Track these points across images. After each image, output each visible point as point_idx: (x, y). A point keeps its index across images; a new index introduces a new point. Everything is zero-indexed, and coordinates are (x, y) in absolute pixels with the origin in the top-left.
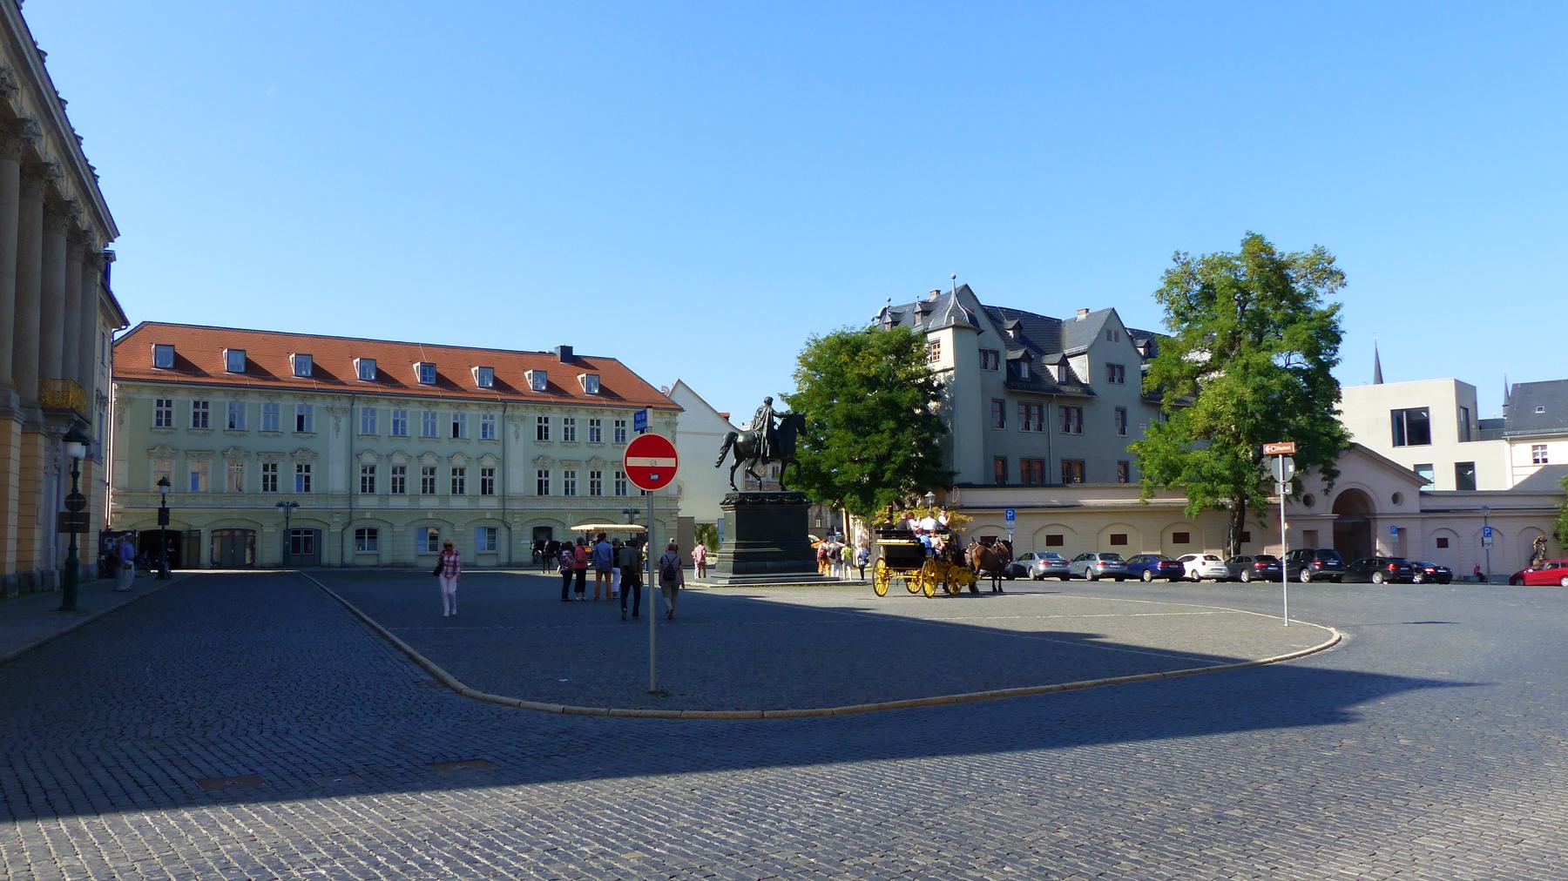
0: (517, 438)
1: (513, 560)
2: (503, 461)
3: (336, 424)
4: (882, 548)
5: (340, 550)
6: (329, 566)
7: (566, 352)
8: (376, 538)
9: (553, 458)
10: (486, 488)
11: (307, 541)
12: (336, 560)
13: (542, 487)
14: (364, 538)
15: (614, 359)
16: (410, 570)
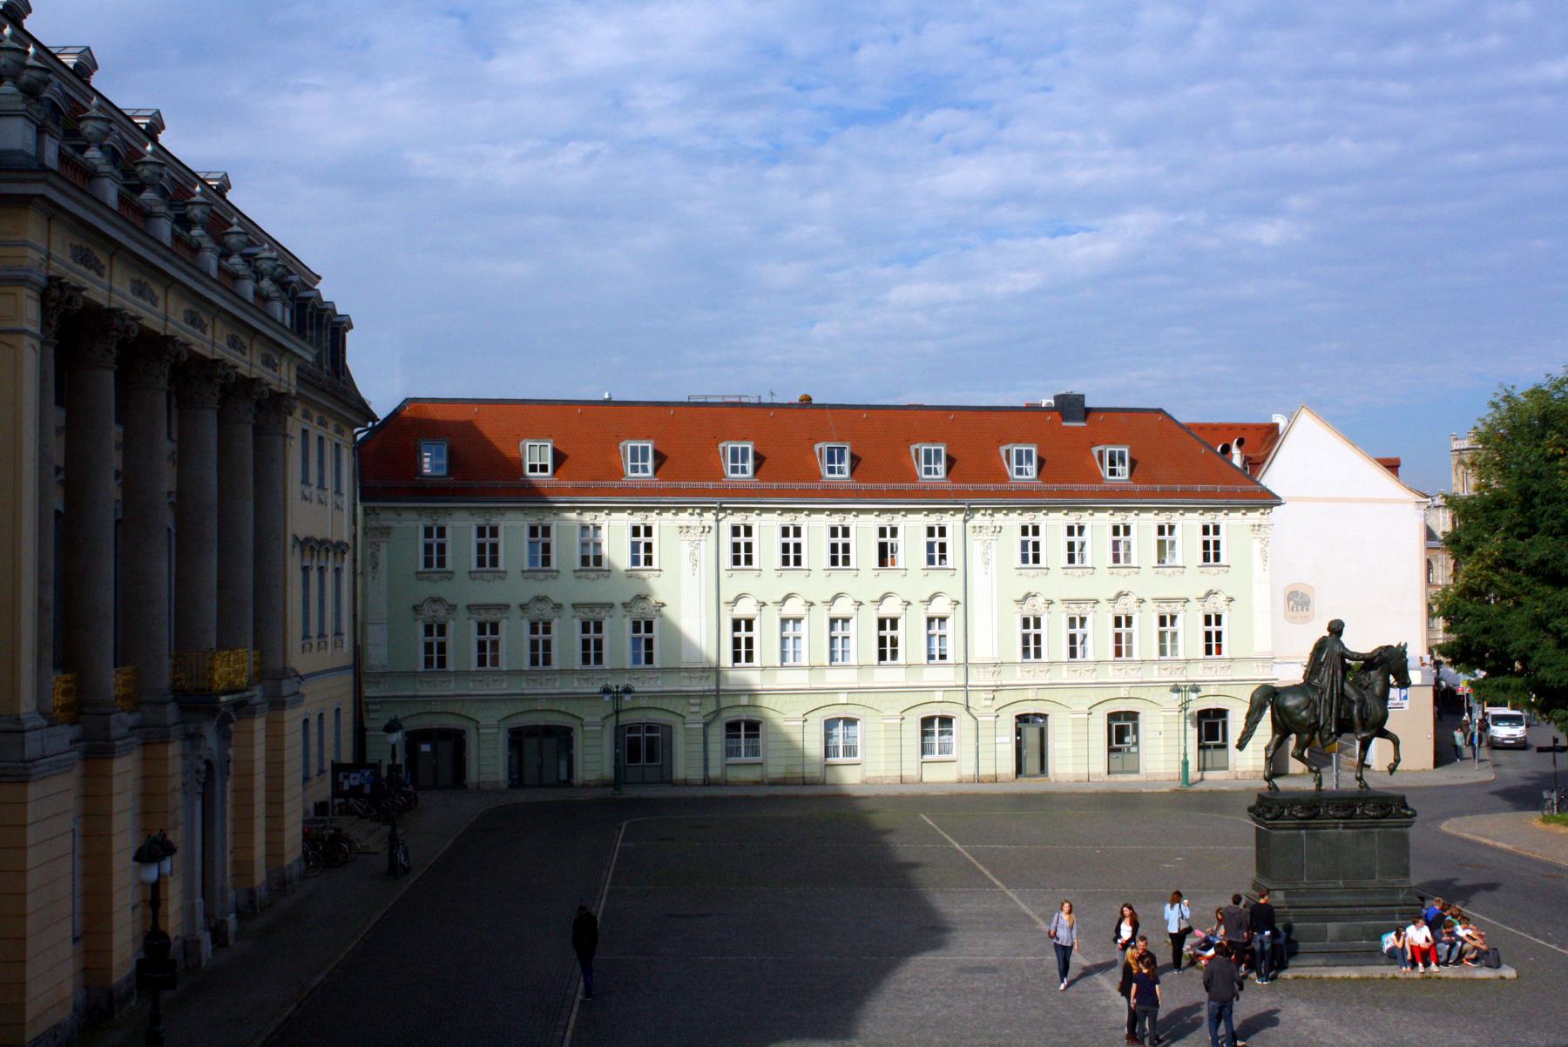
1: (982, 772)
2: (963, 603)
3: (692, 554)
5: (701, 756)
6: (686, 783)
7: (807, 400)
8: (758, 736)
9: (557, 600)
10: (1213, 643)
12: (696, 774)
13: (1031, 646)
14: (739, 736)
15: (1160, 411)
16: (808, 791)
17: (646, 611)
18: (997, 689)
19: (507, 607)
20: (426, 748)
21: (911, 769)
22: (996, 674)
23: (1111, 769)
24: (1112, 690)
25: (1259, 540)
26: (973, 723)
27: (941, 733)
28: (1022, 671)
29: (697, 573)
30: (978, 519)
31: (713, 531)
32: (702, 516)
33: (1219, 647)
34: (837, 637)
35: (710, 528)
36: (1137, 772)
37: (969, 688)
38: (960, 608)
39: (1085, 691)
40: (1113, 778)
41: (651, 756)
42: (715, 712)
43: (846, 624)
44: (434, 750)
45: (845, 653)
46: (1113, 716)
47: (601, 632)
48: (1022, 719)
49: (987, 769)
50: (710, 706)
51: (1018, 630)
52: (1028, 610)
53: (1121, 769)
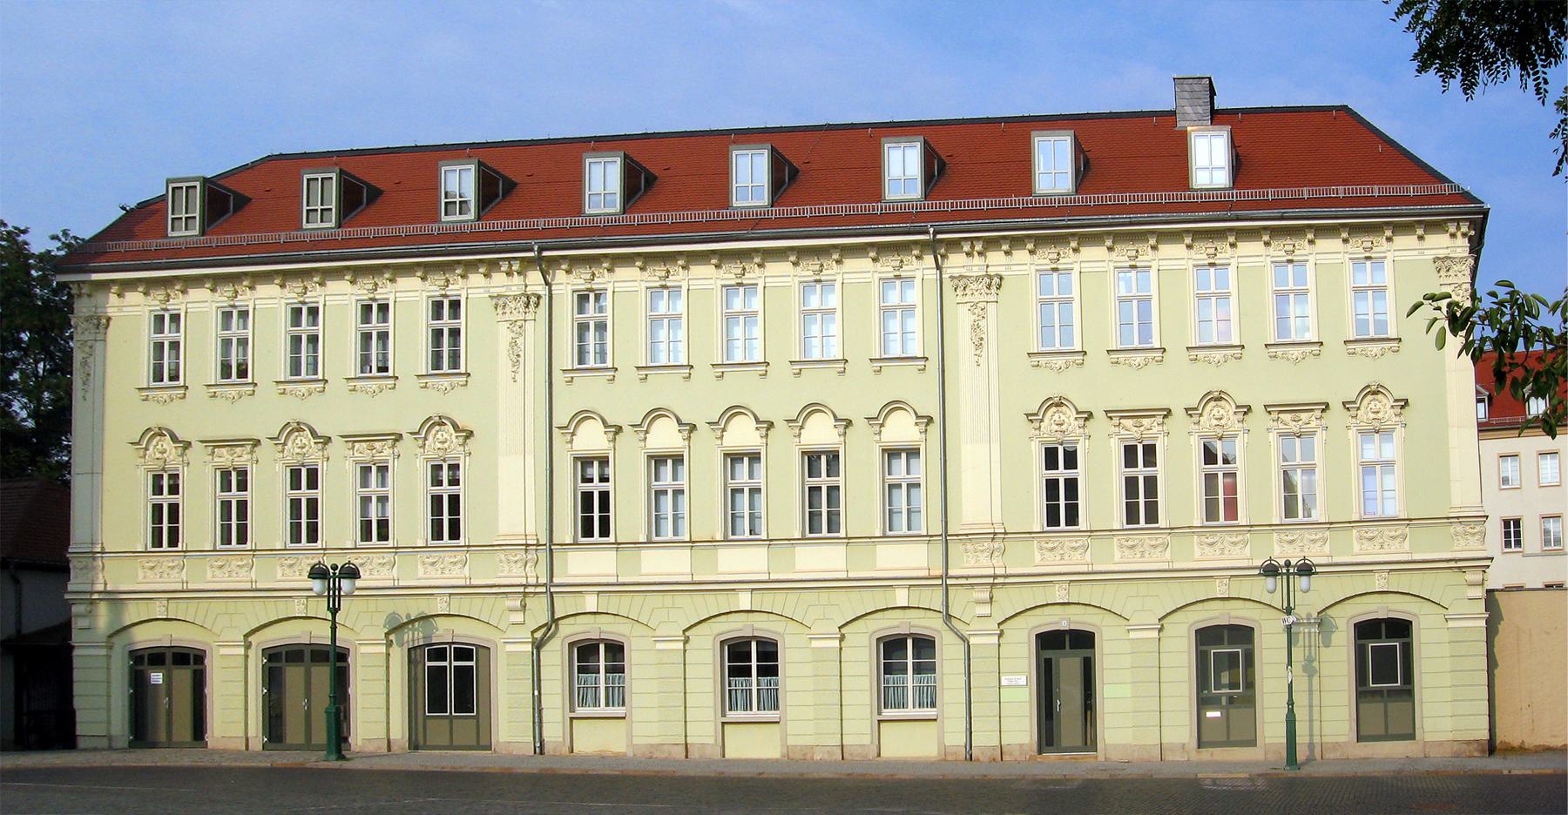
0: (979, 346)
3: (514, 343)
4: (1210, 714)
8: (933, 670)
11: (464, 676)
17: (1380, 416)
18: (995, 583)
19: (1168, 413)
20: (157, 677)
21: (859, 734)
22: (996, 554)
23: (1362, 733)
24: (1186, 584)
25: (507, 324)
26: (961, 648)
27: (918, 669)
28: (1041, 548)
29: (519, 377)
30: (956, 262)
31: (544, 302)
32: (490, 277)
33: (605, 522)
34: (742, 491)
35: (539, 297)
36: (1252, 743)
37: (552, 589)
38: (935, 429)
39: (834, 595)
40: (1207, 754)
41: (464, 703)
42: (546, 624)
43: (913, 461)
44: (168, 679)
45: (913, 516)
46: (1207, 636)
47: (1154, 465)
48: (1049, 642)
49: (984, 739)
50: (538, 612)
51: (1038, 474)
52: (1049, 430)
53: (447, 743)
